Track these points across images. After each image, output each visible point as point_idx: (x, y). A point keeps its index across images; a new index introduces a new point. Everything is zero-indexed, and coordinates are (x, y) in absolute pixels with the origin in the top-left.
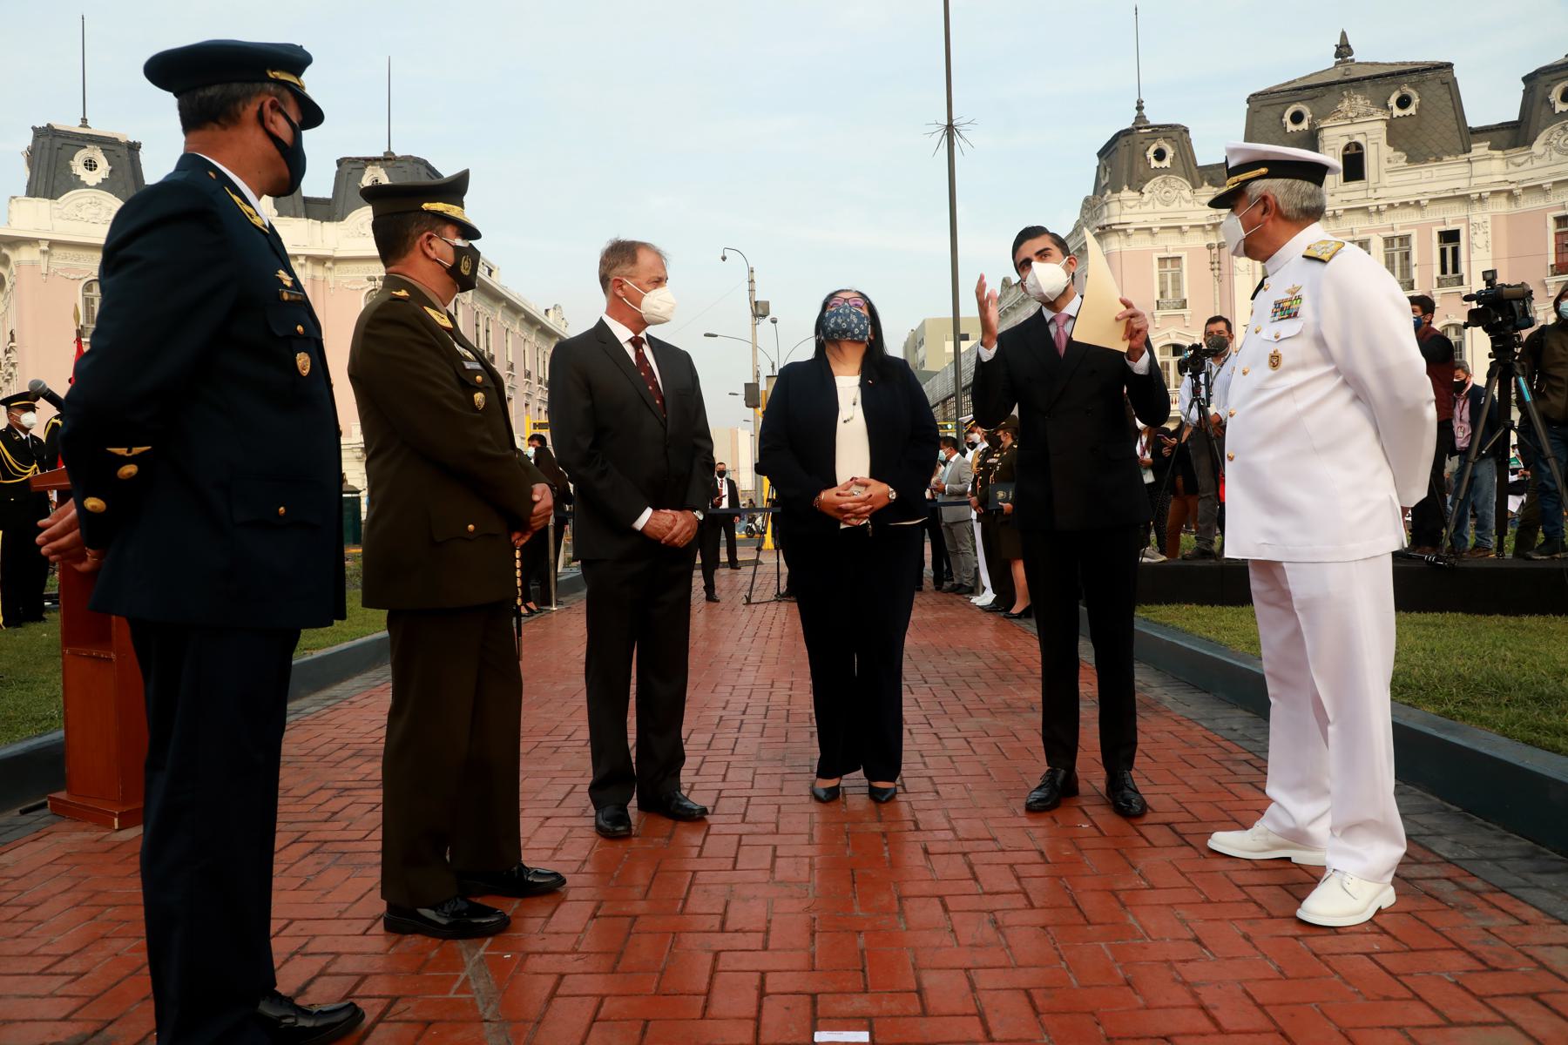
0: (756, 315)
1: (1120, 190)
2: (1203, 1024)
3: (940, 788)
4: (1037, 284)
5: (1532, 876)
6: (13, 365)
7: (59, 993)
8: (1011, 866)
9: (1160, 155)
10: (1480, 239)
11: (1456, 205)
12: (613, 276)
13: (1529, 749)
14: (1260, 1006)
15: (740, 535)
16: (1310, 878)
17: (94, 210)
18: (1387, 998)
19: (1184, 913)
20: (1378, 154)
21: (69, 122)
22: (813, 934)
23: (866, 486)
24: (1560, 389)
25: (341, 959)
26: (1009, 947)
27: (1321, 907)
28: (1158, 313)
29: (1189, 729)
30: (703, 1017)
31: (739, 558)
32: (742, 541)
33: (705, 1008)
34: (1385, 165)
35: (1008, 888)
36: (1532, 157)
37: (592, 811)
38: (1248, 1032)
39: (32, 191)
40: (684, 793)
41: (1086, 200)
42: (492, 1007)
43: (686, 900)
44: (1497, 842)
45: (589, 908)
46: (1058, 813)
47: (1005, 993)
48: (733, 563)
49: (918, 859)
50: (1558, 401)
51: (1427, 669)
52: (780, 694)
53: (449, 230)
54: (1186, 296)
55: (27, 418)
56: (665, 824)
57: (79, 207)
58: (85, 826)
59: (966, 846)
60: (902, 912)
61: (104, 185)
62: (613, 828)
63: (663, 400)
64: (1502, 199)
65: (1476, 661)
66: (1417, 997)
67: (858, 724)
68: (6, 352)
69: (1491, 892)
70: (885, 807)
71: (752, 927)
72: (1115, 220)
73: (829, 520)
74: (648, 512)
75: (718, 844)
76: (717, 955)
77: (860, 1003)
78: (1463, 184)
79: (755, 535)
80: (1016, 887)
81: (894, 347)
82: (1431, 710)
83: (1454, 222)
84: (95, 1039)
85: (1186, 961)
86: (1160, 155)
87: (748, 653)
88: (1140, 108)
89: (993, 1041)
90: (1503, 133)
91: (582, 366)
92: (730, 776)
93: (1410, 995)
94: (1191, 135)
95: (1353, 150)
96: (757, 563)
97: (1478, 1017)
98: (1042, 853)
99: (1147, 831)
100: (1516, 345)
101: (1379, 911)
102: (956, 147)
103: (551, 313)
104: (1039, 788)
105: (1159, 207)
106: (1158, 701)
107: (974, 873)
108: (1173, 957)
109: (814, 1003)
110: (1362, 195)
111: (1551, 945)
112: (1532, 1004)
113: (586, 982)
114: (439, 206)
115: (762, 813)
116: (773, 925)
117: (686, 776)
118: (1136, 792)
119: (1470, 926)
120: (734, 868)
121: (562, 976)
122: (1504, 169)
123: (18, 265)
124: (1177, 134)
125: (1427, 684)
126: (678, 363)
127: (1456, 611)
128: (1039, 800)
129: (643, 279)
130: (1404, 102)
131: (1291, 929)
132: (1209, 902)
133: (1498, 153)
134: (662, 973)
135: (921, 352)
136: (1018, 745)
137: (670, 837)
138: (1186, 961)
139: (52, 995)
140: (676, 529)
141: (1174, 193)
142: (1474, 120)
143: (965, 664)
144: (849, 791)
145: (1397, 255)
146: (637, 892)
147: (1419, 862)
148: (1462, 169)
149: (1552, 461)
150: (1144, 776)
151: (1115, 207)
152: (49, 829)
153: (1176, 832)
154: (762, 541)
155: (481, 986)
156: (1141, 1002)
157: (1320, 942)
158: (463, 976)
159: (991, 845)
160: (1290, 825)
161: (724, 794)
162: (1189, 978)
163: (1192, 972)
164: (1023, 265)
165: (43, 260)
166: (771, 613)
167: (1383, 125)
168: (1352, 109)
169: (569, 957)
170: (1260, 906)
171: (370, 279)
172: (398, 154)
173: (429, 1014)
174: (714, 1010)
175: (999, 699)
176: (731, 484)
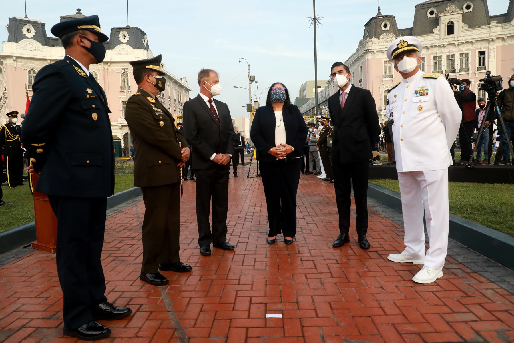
0: (250, 81)
1: (372, 38)
2: (381, 312)
3: (307, 240)
4: (337, 82)
5: (486, 268)
6: (6, 98)
7: (42, 303)
8: (327, 264)
9: (385, 26)
10: (492, 54)
11: (485, 42)
12: (202, 80)
13: (489, 229)
14: (398, 307)
15: (245, 153)
16: (418, 268)
17: (30, 46)
18: (436, 305)
19: (378, 279)
20: (459, 25)
21: (21, 16)
22: (266, 286)
23: (285, 146)
24: (509, 110)
25: (125, 293)
26: (325, 289)
27: (420, 277)
28: (384, 79)
29: (386, 220)
30: (233, 310)
31: (245, 162)
32: (246, 155)
33: (234, 307)
34: (461, 29)
35: (326, 271)
36: (511, 26)
37: (199, 247)
38: (394, 315)
39: (10, 40)
40: (227, 241)
41: (361, 41)
42: (171, 307)
43: (228, 275)
44: (476, 257)
45: (198, 277)
46: (342, 248)
47: (322, 303)
48: (243, 164)
49: (299, 262)
50: (508, 114)
51: (461, 202)
52: (258, 209)
53: (154, 73)
54: (393, 74)
55: (14, 120)
56: (221, 251)
57: (26, 45)
58: (43, 252)
59: (314, 258)
60: (293, 279)
61: (33, 38)
62: (205, 252)
63: (219, 119)
64: (500, 40)
65: (477, 199)
66: (445, 305)
67: (282, 219)
68: (3, 94)
69: (472, 273)
70: (289, 246)
71: (248, 283)
72: (370, 48)
73: (273, 157)
74: (215, 155)
75: (238, 258)
76: (237, 291)
77: (279, 306)
78: (487, 35)
79: (250, 154)
80: (328, 271)
81: (293, 101)
82: (460, 215)
83: (484, 48)
84: (54, 316)
85: (378, 294)
86: (385, 26)
87: (247, 195)
88: (379, 10)
89: (318, 317)
90: (502, 17)
91: (193, 108)
92: (242, 236)
93: (443, 304)
94: (396, 19)
95: (450, 24)
96: (251, 163)
97: (462, 310)
98: (337, 260)
99: (369, 253)
100: (496, 96)
101: (438, 279)
102: (317, 26)
103: (183, 79)
104: (337, 240)
105: (385, 44)
106: (377, 211)
107: (316, 267)
108: (374, 293)
109: (266, 306)
110: (453, 39)
111: (487, 289)
112: (479, 306)
113: (198, 300)
114: (151, 67)
115: (251, 248)
116: (254, 283)
117: (228, 236)
118: (367, 241)
119: (463, 284)
120: (242, 265)
121: (191, 298)
122: (501, 30)
123: (6, 65)
124: (391, 19)
125: (460, 207)
126: (223, 107)
127: (474, 182)
128: (337, 244)
129: (211, 81)
130: (468, 7)
131: (410, 284)
132: (386, 275)
133: (500, 25)
134: (221, 297)
135: (305, 92)
136: (332, 225)
137: (223, 255)
138: (378, 294)
139: (40, 304)
140: (223, 159)
141: (390, 39)
142: (491, 14)
143: (316, 199)
144: (278, 240)
145: (464, 59)
146: (213, 272)
147: (452, 264)
148: (487, 30)
149: (506, 134)
150: (369, 236)
151: (370, 43)
152: (33, 253)
153: (378, 253)
154: (253, 155)
155: (167, 301)
156: (363, 306)
157: (418, 288)
158: (161, 298)
159: (322, 258)
160: (413, 252)
161: (240, 241)
162: (378, 299)
163: (379, 297)
164: (333, 75)
165: (14, 63)
166: (255, 181)
167: (461, 15)
168: (450, 10)
169: (193, 292)
170: (402, 277)
171: (122, 69)
172: (131, 26)
173: (152, 310)
174: (236, 308)
175: (327, 211)
176: (243, 138)
